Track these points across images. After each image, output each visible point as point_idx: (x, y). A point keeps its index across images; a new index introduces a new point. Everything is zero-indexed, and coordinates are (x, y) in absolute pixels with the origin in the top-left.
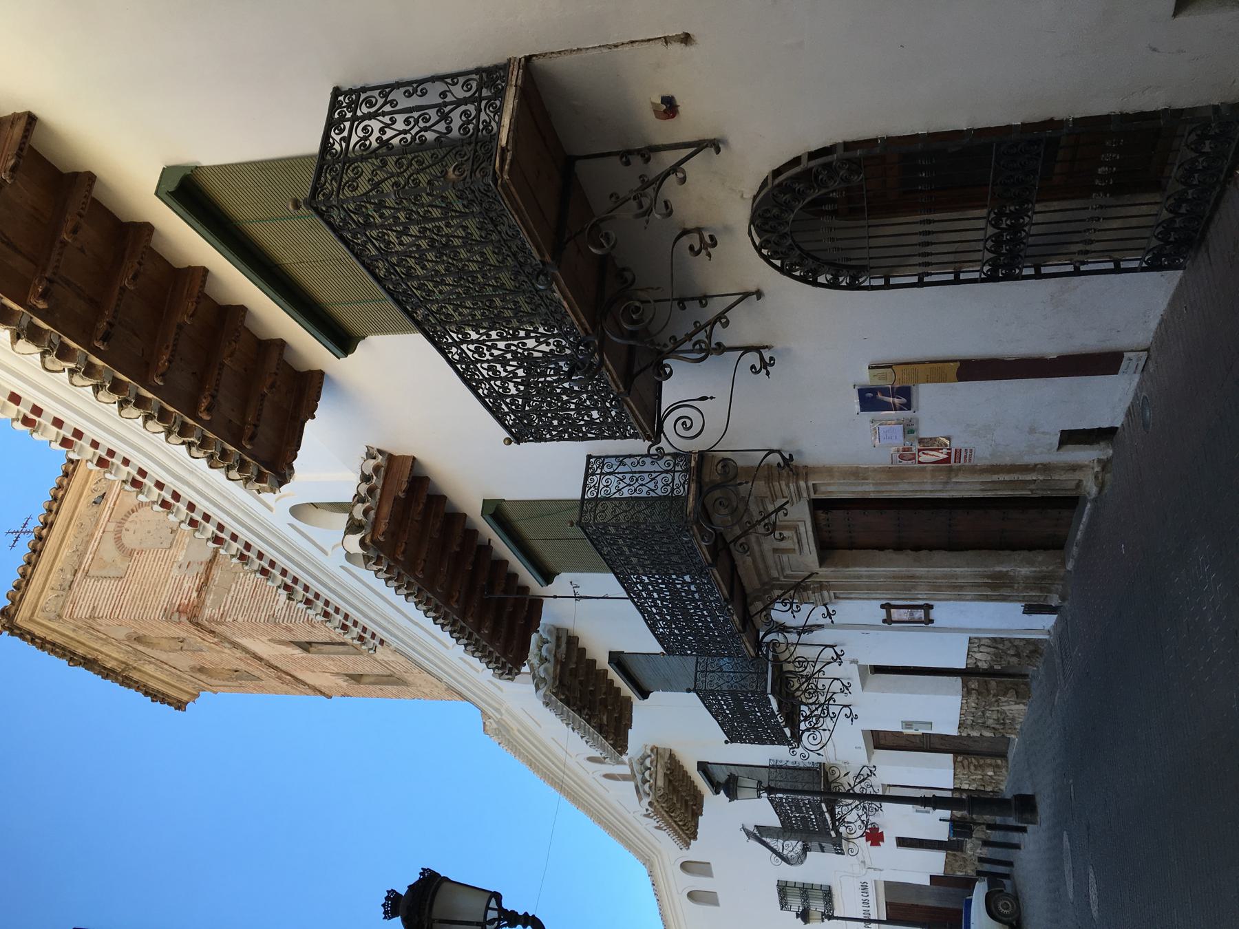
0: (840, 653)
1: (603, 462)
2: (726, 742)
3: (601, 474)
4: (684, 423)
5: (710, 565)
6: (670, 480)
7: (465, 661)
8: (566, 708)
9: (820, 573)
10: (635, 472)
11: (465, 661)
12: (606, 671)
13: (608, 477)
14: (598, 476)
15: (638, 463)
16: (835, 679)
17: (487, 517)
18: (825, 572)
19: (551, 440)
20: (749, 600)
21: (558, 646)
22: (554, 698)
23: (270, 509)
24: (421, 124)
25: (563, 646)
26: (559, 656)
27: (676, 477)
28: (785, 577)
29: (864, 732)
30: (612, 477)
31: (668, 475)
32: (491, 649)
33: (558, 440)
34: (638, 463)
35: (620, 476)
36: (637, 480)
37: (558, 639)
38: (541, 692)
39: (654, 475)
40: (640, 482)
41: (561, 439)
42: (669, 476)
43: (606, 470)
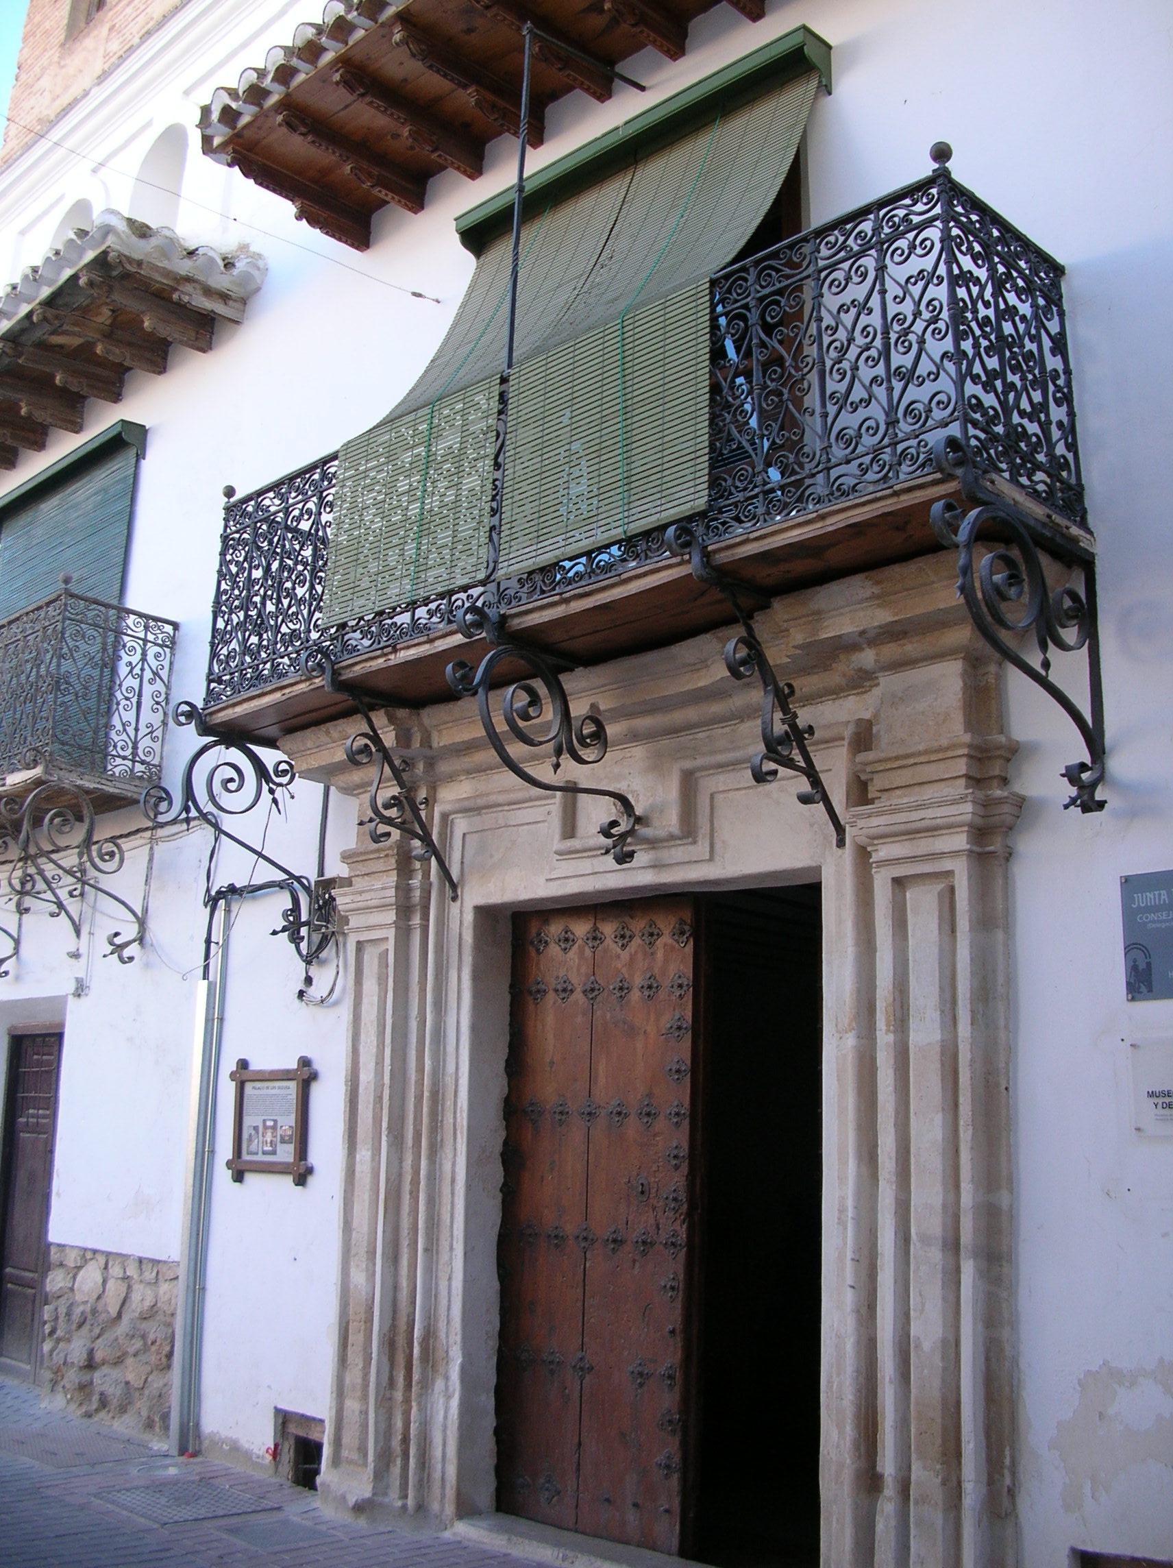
0: (127, 953)
1: (167, 646)
2: (230, 492)
3: (145, 641)
4: (231, 780)
5: (336, 673)
6: (122, 753)
7: (52, 206)
8: (46, 292)
9: (455, 908)
10: (140, 695)
11: (52, 206)
12: (77, 428)
13: (139, 651)
14: (142, 635)
15: (158, 703)
16: (17, 942)
17: (119, 428)
18: (462, 919)
19: (224, 562)
20: (402, 713)
21: (208, 292)
22: (90, 255)
23: (187, 93)
24: (984, 343)
25: (207, 304)
26: (188, 288)
27: (126, 762)
28: (445, 817)
29: (818, 869)
30: (138, 656)
31: (130, 751)
32: (328, 57)
33: (220, 572)
34: (158, 703)
35: (137, 670)
36: (127, 699)
37: (224, 297)
38: (122, 227)
39: (131, 730)
40: (123, 702)
41: (221, 575)
42: (128, 753)
43: (152, 650)
